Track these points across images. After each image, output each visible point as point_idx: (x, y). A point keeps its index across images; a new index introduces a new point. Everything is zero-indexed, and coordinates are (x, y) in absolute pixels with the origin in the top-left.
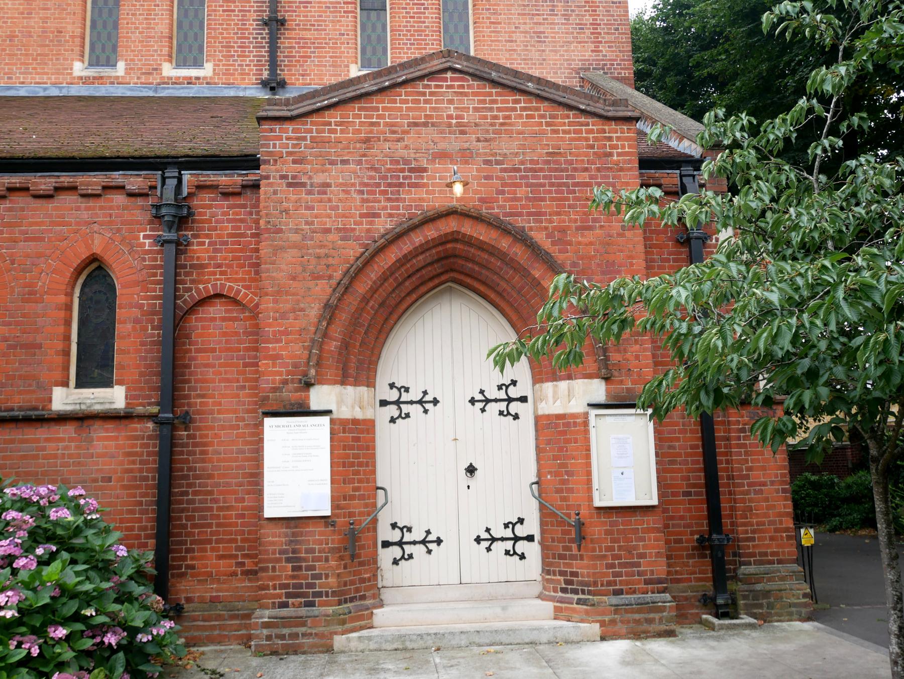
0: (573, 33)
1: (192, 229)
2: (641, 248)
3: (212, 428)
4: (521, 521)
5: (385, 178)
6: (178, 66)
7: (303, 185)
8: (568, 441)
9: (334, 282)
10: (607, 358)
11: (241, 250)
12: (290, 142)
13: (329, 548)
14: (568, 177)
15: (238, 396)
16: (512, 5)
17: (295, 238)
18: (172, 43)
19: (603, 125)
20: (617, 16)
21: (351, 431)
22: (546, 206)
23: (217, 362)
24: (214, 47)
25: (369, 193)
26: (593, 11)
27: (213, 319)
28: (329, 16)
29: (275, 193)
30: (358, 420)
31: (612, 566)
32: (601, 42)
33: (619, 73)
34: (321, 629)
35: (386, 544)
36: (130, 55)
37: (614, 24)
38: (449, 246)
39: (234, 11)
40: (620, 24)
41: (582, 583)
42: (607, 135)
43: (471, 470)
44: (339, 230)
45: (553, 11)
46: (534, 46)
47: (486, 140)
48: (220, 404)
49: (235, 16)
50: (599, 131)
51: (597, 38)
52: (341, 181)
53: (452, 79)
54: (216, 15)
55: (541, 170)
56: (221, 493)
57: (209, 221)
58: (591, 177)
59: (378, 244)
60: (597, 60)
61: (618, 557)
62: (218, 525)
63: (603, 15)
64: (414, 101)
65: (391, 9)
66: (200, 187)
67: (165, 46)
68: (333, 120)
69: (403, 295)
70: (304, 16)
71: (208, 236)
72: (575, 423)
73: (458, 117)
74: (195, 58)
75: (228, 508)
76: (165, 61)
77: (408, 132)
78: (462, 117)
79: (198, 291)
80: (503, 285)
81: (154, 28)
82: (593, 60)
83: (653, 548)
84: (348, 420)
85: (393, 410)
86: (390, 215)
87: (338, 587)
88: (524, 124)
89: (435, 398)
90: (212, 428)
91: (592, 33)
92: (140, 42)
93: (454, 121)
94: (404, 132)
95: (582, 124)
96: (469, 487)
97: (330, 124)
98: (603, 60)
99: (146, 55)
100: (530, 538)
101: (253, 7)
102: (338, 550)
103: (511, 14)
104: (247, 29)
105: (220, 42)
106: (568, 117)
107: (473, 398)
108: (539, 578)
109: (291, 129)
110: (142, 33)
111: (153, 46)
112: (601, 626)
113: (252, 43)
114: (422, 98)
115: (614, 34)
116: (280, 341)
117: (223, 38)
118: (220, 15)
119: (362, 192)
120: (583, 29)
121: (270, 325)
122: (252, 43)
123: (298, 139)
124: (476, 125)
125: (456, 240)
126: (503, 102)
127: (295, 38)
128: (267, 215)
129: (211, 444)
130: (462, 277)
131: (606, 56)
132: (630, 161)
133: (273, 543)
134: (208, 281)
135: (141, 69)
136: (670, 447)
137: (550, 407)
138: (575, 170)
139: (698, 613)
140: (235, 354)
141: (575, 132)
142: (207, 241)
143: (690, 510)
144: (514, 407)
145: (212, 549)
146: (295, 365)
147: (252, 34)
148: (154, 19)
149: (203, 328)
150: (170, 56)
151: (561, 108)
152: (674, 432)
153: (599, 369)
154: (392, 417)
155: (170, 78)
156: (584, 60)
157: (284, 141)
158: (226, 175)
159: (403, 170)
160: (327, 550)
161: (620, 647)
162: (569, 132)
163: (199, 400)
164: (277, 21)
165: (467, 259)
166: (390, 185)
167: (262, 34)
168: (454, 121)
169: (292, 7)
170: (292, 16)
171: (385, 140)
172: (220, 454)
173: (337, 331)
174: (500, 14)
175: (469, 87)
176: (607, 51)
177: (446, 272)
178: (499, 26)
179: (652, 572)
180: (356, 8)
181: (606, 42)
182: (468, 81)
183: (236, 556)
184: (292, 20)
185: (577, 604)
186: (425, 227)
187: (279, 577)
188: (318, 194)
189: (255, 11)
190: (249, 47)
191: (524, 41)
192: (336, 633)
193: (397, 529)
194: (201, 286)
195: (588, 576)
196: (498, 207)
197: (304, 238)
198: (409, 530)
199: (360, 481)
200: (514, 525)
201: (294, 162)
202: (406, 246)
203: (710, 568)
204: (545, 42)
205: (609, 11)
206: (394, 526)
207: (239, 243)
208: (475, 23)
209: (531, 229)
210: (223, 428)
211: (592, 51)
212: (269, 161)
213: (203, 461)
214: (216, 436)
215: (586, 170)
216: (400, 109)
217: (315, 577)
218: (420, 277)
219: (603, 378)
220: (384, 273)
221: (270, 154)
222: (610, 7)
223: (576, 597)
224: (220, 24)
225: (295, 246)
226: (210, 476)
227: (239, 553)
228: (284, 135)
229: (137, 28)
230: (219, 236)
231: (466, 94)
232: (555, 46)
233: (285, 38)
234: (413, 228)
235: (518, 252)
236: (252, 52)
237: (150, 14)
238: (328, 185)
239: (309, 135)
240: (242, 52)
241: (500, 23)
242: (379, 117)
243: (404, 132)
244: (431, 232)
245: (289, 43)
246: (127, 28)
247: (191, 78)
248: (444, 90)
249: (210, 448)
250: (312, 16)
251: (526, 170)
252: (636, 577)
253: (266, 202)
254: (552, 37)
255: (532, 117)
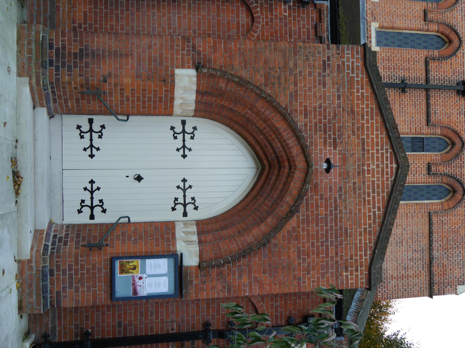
0: (402, 263)
1: (294, 5)
2: (286, 291)
3: (169, 12)
4: (104, 211)
5: (330, 123)
6: (377, 32)
7: (324, 71)
8: (157, 240)
9: (263, 88)
10: (213, 267)
11: (281, 35)
12: (350, 64)
13: (88, 77)
14: (332, 242)
15: (189, 29)
16: (417, 226)
17: (291, 64)
18: (389, 29)
19: (366, 265)
20: (413, 290)
21: (166, 96)
22: (313, 228)
23: (211, 17)
24: (389, 52)
25: (320, 112)
26: (416, 275)
27: (238, 16)
28: (408, 118)
29: (319, 53)
30: (173, 102)
31: (70, 269)
32: (398, 280)
33: (379, 291)
34: (34, 69)
35: (91, 121)
36: (382, 5)
37: (408, 288)
38: (286, 163)
39: (409, 64)
40: (408, 292)
41: (59, 249)
42: (359, 268)
43: (139, 178)
44: (296, 91)
45: (415, 251)
46: (394, 240)
47: (354, 188)
48: (184, 18)
49: (406, 64)
50: (361, 263)
51: (400, 278)
52: (327, 94)
53: (392, 168)
54: (406, 53)
55: (336, 224)
56: (127, 16)
57: (299, 16)
58: (332, 257)
59: (288, 116)
60: (387, 278)
61: (76, 274)
62: (106, 14)
63: (413, 282)
64: (377, 142)
65: (413, 154)
66: (320, 12)
67: (388, 24)
68: (364, 91)
69: (254, 134)
70: (407, 104)
71: (290, 15)
72: (170, 245)
73: (368, 170)
74: (381, 42)
75: (117, 20)
76: (380, 24)
77: (358, 138)
78: (368, 173)
79: (256, 7)
80: (261, 200)
81: (398, 18)
82: (387, 276)
83: (82, 298)
84: (174, 94)
85: (179, 129)
86: (306, 125)
87: (62, 82)
88: (365, 213)
89: (186, 156)
90: (169, 12)
91: (403, 275)
92: (390, 10)
93: (366, 168)
94: (358, 135)
95: (366, 251)
96: (128, 177)
97: (362, 89)
98: (387, 281)
99: (382, 14)
100: (92, 217)
101: (412, 75)
102: (87, 84)
103: (412, 226)
104: (399, 71)
105: (391, 55)
106: (370, 242)
107: (186, 181)
108: (64, 222)
109: (358, 64)
110: (395, 12)
111: (388, 18)
112: (28, 260)
113: (391, 73)
114: (379, 148)
115: (403, 289)
116: (226, 52)
117: (393, 57)
118: (406, 56)
119: (320, 107)
120: (405, 269)
121: (235, 45)
122: (391, 73)
123: (353, 68)
124: (364, 182)
125: (290, 168)
126: (379, 200)
127: (395, 98)
128: (305, 47)
129: (159, 11)
130: (265, 174)
131: (390, 283)
132: (342, 283)
133: (93, 41)
134: (262, 14)
135: (375, 10)
136: (152, 313)
137: (180, 232)
138: (337, 247)
139: (36, 331)
140: (216, 29)
141: (361, 247)
142: (287, 14)
143: (108, 326)
144: (180, 208)
145: (90, 9)
146: (209, 61)
147: (396, 74)
148: (403, 19)
149: (233, 10)
150: (382, 27)
151: (376, 238)
152: (162, 316)
153: (206, 261)
154: (174, 128)
155: (370, 26)
156: (387, 270)
157: (351, 60)
158: (327, 27)
159: (334, 134)
160: (87, 76)
161: (13, 268)
162: (360, 243)
163: (187, 5)
164: (404, 88)
165: (278, 176)
166: (325, 125)
167: (397, 79)
168: (366, 168)
169: (412, 97)
170: (407, 97)
171: (353, 124)
172: (153, 16)
173: (232, 87)
174: (412, 219)
175: (387, 178)
176: (392, 284)
177: (269, 163)
178: (405, 219)
179: (65, 297)
180: (413, 134)
181: (398, 283)
182: (391, 177)
183: (85, 23)
184: (405, 97)
185: (45, 244)
186: (299, 147)
187: (70, 44)
188: (319, 80)
189: (409, 76)
190: (389, 72)
191: (397, 233)
192: (30, 79)
193: (101, 129)
194: (259, 9)
195: (63, 252)
196: (312, 195)
197: (291, 70)
198: (100, 137)
199: (133, 101)
200: (101, 206)
201: (338, 66)
202: (287, 135)
203: (68, 340)
204: (397, 246)
205: (416, 285)
206: (103, 127)
207: (286, 34)
208: (407, 204)
209: (298, 217)
210: (169, 19)
211: (392, 275)
212: (339, 50)
213: (148, 6)
214: (164, 15)
215: (337, 254)
216: (372, 134)
217: (69, 67)
218: (266, 145)
219: (200, 264)
220: (269, 120)
221: (343, 51)
222: (418, 286)
223: (50, 244)
224: (401, 56)
225: (286, 64)
226: (138, 10)
227: (88, 26)
228: (355, 60)
229: (397, 9)
230: (290, 21)
231: (383, 176)
232: (394, 253)
233: (395, 92)
234: (299, 139)
235: (283, 209)
236: (386, 74)
237: (405, 17)
238: (324, 86)
239: (355, 75)
240: (386, 68)
241: (407, 219)
242: (367, 120)
243: (358, 135)
244: (295, 151)
245: (392, 95)
246: (397, 4)
247: (371, 38)
248: (385, 162)
249: (156, 11)
250: (407, 108)
251: (336, 214)
252: (62, 286)
253: (313, 47)
254: (400, 251)
255: (370, 219)
